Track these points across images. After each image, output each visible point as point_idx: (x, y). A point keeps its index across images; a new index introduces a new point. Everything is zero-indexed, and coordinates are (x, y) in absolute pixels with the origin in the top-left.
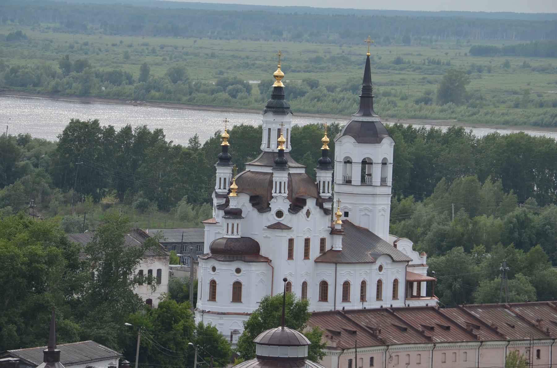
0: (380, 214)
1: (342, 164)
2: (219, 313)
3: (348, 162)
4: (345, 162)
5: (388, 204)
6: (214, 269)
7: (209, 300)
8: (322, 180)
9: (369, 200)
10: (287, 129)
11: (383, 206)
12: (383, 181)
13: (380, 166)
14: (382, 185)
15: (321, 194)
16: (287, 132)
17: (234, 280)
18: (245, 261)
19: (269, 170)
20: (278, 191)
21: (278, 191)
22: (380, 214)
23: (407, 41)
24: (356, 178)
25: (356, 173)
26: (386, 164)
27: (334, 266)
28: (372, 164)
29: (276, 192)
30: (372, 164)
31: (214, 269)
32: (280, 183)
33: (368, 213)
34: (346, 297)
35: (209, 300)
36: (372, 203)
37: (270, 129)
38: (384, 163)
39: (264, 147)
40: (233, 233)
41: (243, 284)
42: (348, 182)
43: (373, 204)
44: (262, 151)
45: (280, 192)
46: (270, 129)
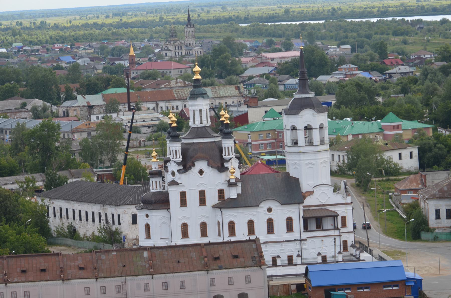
0: (322, 166)
1: (290, 130)
2: (284, 241)
3: (294, 129)
4: (292, 130)
5: (328, 158)
6: (147, 216)
7: (146, 238)
8: (227, 146)
9: (312, 156)
10: (207, 109)
11: (310, 161)
12: (322, 141)
13: (318, 130)
14: (321, 144)
15: (224, 157)
16: (207, 111)
17: (268, 217)
18: (148, 209)
19: (219, 139)
20: (227, 154)
21: (227, 154)
22: (322, 166)
23: (63, 43)
24: (301, 140)
25: (301, 137)
26: (322, 128)
27: (298, 205)
28: (312, 129)
29: (225, 155)
30: (312, 129)
31: (147, 216)
32: (176, 151)
33: (312, 166)
34: (204, 233)
35: (146, 238)
36: (314, 158)
37: (194, 110)
38: (321, 128)
39: (191, 124)
40: (156, 188)
41: (189, 225)
42: (296, 143)
43: (316, 159)
44: (190, 127)
45: (229, 155)
46: (194, 110)
